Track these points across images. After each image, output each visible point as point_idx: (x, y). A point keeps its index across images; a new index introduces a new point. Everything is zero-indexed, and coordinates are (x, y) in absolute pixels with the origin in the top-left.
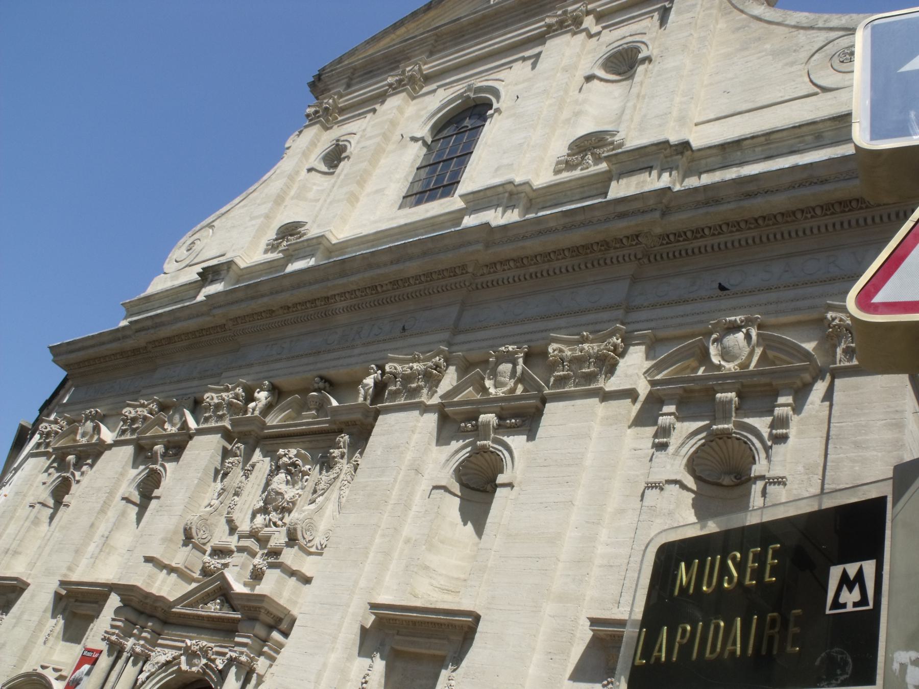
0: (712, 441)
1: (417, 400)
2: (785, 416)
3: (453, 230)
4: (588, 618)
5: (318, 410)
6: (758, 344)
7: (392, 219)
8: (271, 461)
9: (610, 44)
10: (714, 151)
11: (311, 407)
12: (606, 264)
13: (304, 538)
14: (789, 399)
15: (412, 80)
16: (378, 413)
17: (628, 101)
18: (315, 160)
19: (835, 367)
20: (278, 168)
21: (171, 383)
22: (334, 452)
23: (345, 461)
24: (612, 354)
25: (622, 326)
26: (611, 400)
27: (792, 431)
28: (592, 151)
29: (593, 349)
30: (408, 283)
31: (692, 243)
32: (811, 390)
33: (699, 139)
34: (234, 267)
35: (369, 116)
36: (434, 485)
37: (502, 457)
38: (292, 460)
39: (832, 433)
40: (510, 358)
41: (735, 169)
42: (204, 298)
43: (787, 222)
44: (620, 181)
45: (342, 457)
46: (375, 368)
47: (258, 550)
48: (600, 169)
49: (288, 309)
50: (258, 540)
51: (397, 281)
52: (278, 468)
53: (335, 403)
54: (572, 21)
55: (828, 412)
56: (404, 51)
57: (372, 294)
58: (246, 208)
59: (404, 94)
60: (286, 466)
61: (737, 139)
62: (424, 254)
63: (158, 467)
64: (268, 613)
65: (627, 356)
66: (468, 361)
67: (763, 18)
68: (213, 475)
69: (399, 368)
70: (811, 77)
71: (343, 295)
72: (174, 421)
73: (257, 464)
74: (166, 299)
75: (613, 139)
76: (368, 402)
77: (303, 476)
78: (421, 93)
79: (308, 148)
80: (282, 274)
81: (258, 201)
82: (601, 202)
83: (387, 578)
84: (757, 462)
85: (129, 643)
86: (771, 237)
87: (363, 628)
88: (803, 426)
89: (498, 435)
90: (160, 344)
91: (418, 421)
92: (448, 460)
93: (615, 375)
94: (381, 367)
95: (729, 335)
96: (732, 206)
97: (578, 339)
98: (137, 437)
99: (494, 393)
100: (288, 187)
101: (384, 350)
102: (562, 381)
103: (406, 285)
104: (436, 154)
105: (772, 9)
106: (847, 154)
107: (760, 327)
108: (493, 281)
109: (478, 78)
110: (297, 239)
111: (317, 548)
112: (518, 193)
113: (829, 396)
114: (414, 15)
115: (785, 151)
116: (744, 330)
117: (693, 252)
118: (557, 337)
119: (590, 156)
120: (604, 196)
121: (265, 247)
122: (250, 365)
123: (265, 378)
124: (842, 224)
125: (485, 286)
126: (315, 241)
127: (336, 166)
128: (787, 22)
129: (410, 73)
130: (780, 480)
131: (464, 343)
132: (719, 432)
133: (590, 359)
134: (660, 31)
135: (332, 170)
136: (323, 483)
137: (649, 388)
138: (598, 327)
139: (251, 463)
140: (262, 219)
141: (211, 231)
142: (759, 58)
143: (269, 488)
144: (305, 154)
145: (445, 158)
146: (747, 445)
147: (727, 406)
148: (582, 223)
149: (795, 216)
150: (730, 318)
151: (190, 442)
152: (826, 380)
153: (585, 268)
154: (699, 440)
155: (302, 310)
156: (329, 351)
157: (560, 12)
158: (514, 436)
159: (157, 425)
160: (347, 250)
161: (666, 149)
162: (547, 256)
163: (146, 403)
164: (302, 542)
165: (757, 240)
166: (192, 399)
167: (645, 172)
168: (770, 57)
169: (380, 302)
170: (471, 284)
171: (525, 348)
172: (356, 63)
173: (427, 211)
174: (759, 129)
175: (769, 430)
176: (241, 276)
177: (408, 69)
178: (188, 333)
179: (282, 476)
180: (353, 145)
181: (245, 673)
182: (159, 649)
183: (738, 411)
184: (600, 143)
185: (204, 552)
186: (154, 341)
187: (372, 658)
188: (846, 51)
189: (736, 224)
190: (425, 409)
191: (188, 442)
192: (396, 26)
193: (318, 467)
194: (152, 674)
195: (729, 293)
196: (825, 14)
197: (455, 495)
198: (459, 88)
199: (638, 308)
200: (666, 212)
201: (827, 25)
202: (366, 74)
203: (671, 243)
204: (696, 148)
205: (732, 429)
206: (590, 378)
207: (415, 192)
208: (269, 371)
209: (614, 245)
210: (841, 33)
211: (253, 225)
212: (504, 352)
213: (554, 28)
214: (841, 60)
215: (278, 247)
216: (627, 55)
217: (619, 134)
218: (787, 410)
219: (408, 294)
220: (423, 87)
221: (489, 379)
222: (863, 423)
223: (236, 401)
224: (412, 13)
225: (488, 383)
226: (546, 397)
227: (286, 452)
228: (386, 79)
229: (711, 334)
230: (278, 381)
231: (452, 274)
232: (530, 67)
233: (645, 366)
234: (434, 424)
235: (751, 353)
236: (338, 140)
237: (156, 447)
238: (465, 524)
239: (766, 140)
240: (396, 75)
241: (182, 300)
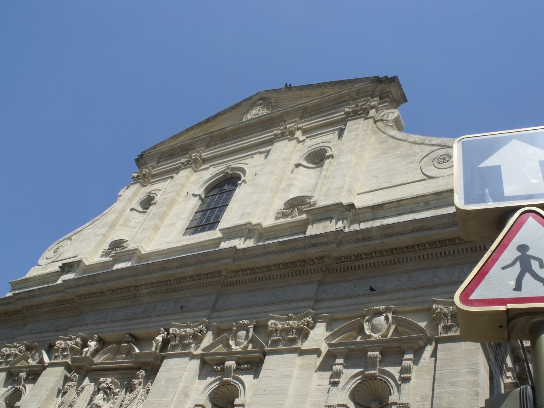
0: (365, 381)
1: (188, 351)
2: (408, 366)
3: (214, 250)
5: (126, 355)
6: (393, 323)
7: (179, 241)
8: (95, 385)
9: (310, 147)
10: (368, 210)
11: (122, 352)
12: (304, 273)
14: (411, 356)
15: (195, 161)
16: (163, 358)
17: (319, 179)
18: (136, 204)
19: (438, 337)
20: (113, 207)
21: (35, 333)
22: (135, 381)
23: (141, 387)
24: (306, 327)
25: (312, 311)
26: (305, 355)
27: (413, 375)
28: (297, 207)
29: (295, 324)
30: (186, 280)
31: (354, 263)
32: (424, 351)
33: (360, 202)
34: (82, 264)
35: (169, 180)
36: (196, 404)
37: (238, 388)
38: (108, 385)
39: (436, 377)
40: (245, 328)
41: (380, 220)
42: (62, 282)
43: (410, 252)
44: (314, 225)
45: (140, 384)
46: (163, 330)
48: (303, 217)
49: (113, 292)
51: (180, 278)
52: (99, 390)
53: (137, 351)
54: (289, 133)
55: (434, 364)
56: (192, 144)
57: (164, 285)
59: (190, 169)
60: (104, 388)
61: (381, 203)
62: (197, 263)
63: (21, 387)
65: (315, 329)
66: (220, 329)
67: (395, 137)
68: (57, 393)
69: (178, 331)
70: (422, 170)
71: (147, 285)
72: (35, 358)
73: (86, 387)
74: (38, 281)
75: (310, 201)
76: (158, 351)
77: (114, 396)
78: (200, 169)
79: (132, 197)
80: (111, 270)
81: (100, 226)
82: (302, 237)
84: (392, 394)
86: (401, 260)
88: (419, 372)
89: (236, 374)
90: (31, 309)
91: (188, 364)
92: (205, 389)
93: (307, 340)
94: (167, 330)
96: (378, 242)
97: (286, 317)
98: (9, 367)
99: (234, 348)
100: (118, 219)
101: (170, 320)
103: (185, 281)
104: (207, 205)
105: (401, 132)
106: (443, 214)
107: (394, 313)
108: (236, 281)
109: (233, 162)
110: (121, 250)
113: (434, 354)
114: (199, 124)
115: (409, 211)
116: (384, 315)
117: (355, 268)
118: (273, 316)
119: (296, 210)
120: (304, 233)
121: (102, 253)
122: (87, 325)
123: (96, 333)
124: (441, 253)
125: (232, 284)
126: (132, 252)
127: (148, 208)
128: (408, 140)
129: (195, 157)
130: (406, 405)
131: (218, 317)
132: (369, 376)
133: (293, 330)
134: (338, 141)
135: (145, 211)
136: (127, 400)
137: (328, 348)
138: (298, 311)
139: (82, 386)
140: (101, 237)
141: (69, 241)
142: (393, 159)
143: (92, 402)
144: (130, 200)
145: (212, 207)
146: (386, 384)
147: (374, 359)
148: (290, 249)
149: (414, 248)
150: (377, 307)
151: (44, 371)
152: (432, 345)
153: (291, 275)
154: (357, 381)
155: (121, 292)
156: (136, 319)
157: (282, 128)
158: (246, 375)
159: (24, 359)
160: (150, 258)
161: (340, 208)
162: (269, 268)
165: (392, 262)
166: (48, 344)
167: (328, 221)
168: (400, 158)
169: (169, 290)
170: (223, 282)
171: (254, 322)
172: (164, 150)
173: (200, 238)
174: (394, 198)
175: (399, 375)
176: (86, 270)
177: (193, 155)
178: (49, 303)
179: (101, 395)
180: (158, 197)
183: (381, 363)
186: (28, 307)
188: (441, 157)
190: (192, 357)
191: (42, 371)
192: (188, 130)
193: (124, 390)
195: (376, 293)
196: (429, 137)
198: (222, 168)
199: (323, 300)
201: (430, 143)
202: (169, 156)
203: (343, 262)
204: (358, 208)
205: (377, 374)
206: (293, 341)
207: (193, 226)
208: (98, 329)
209: (309, 262)
211: (95, 240)
212: (242, 324)
213: (278, 136)
214: (439, 162)
215: (109, 254)
216: (320, 154)
217: (313, 198)
218: (410, 363)
219: (185, 286)
220: (202, 165)
221: (232, 340)
222: (455, 371)
223: (76, 346)
224: (198, 123)
225: (231, 343)
226: (266, 352)
227: (105, 380)
228: (180, 160)
229: (365, 316)
230: (103, 336)
231: (212, 276)
232: (264, 157)
233: (326, 335)
234: (197, 366)
235: (389, 328)
236: (150, 193)
237: (21, 374)
239: (398, 205)
240: (187, 158)
241: (48, 282)
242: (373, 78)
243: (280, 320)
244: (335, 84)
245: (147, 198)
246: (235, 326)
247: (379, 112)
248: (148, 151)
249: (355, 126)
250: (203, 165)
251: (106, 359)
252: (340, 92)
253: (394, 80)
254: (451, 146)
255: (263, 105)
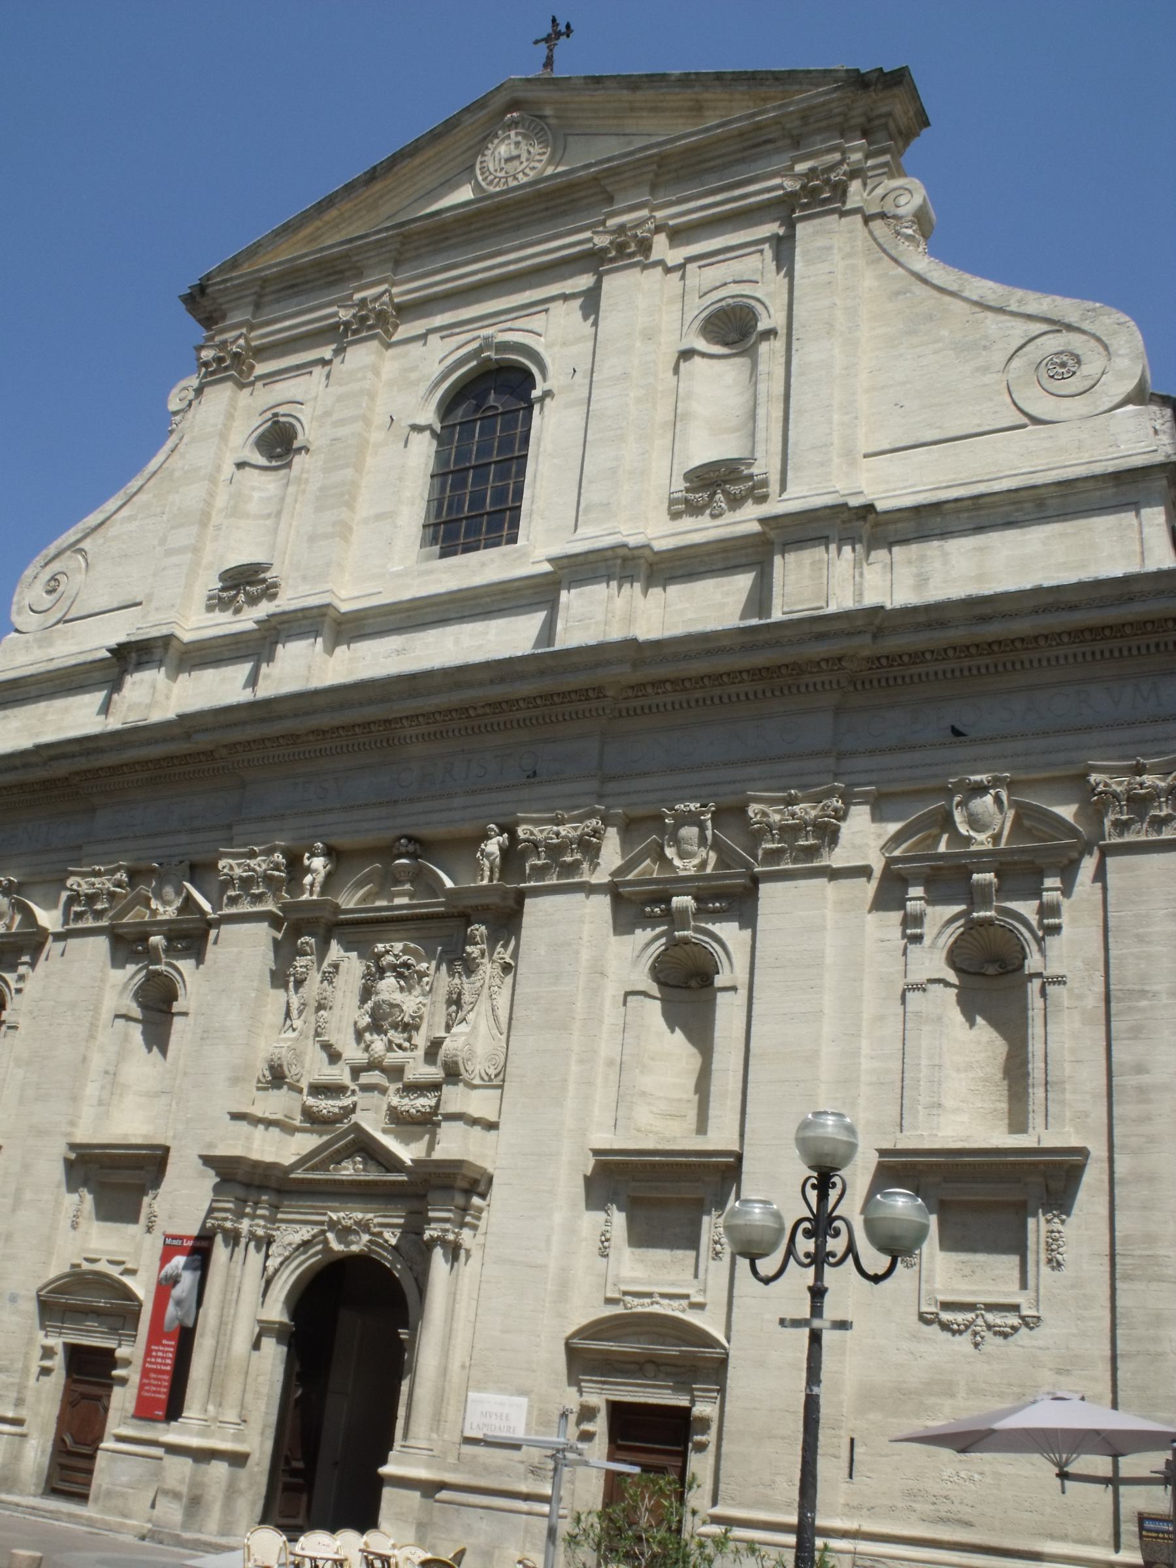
0: (971, 929)
1: (576, 880)
4: (876, 1150)
10: (905, 514)
13: (467, 1071)
16: (520, 897)
23: (486, 960)
27: (1064, 920)
34: (174, 643)
37: (712, 950)
39: (1110, 924)
40: (692, 819)
45: (483, 955)
47: (387, 1084)
50: (383, 1070)
52: (381, 971)
53: (449, 884)
58: (137, 523)
60: (394, 968)
62: (542, 673)
64: (464, 1177)
65: (848, 819)
67: (930, 279)
70: (1013, 395)
79: (225, 425)
83: (596, 1111)
85: (245, 1225)
87: (585, 1176)
93: (839, 846)
94: (509, 829)
95: (975, 798)
100: (212, 495)
102: (774, 856)
111: (482, 1079)
112: (634, 558)
113: (1100, 875)
114: (350, 188)
115: (999, 521)
123: (318, 838)
126: (315, 611)
128: (966, 294)
142: (936, 352)
154: (957, 929)
160: (365, 622)
161: (843, 513)
162: (717, 678)
163: (102, 869)
164: (465, 1075)
166: (188, 863)
181: (450, 1251)
182: (283, 1226)
184: (732, 476)
185: (300, 1091)
187: (606, 1211)
188: (1055, 360)
189: (965, 649)
190: (590, 889)
194: (287, 1259)
197: (655, 998)
199: (853, 754)
200: (878, 634)
201: (1023, 310)
203: (883, 667)
206: (811, 852)
210: (1045, 327)
217: (757, 462)
218: (1056, 896)
221: (670, 846)
225: (670, 852)
232: (579, 314)
238: (673, 1031)
239: (974, 504)
241: (81, 687)
242: (843, 74)
243: (771, 802)
244: (733, 80)
245: (271, 427)
246: (668, 816)
247: (869, 188)
248: (218, 275)
249: (821, 242)
250: (402, 324)
251: (364, 899)
252: (754, 115)
253: (898, 79)
254: (1076, 325)
255: (523, 127)
